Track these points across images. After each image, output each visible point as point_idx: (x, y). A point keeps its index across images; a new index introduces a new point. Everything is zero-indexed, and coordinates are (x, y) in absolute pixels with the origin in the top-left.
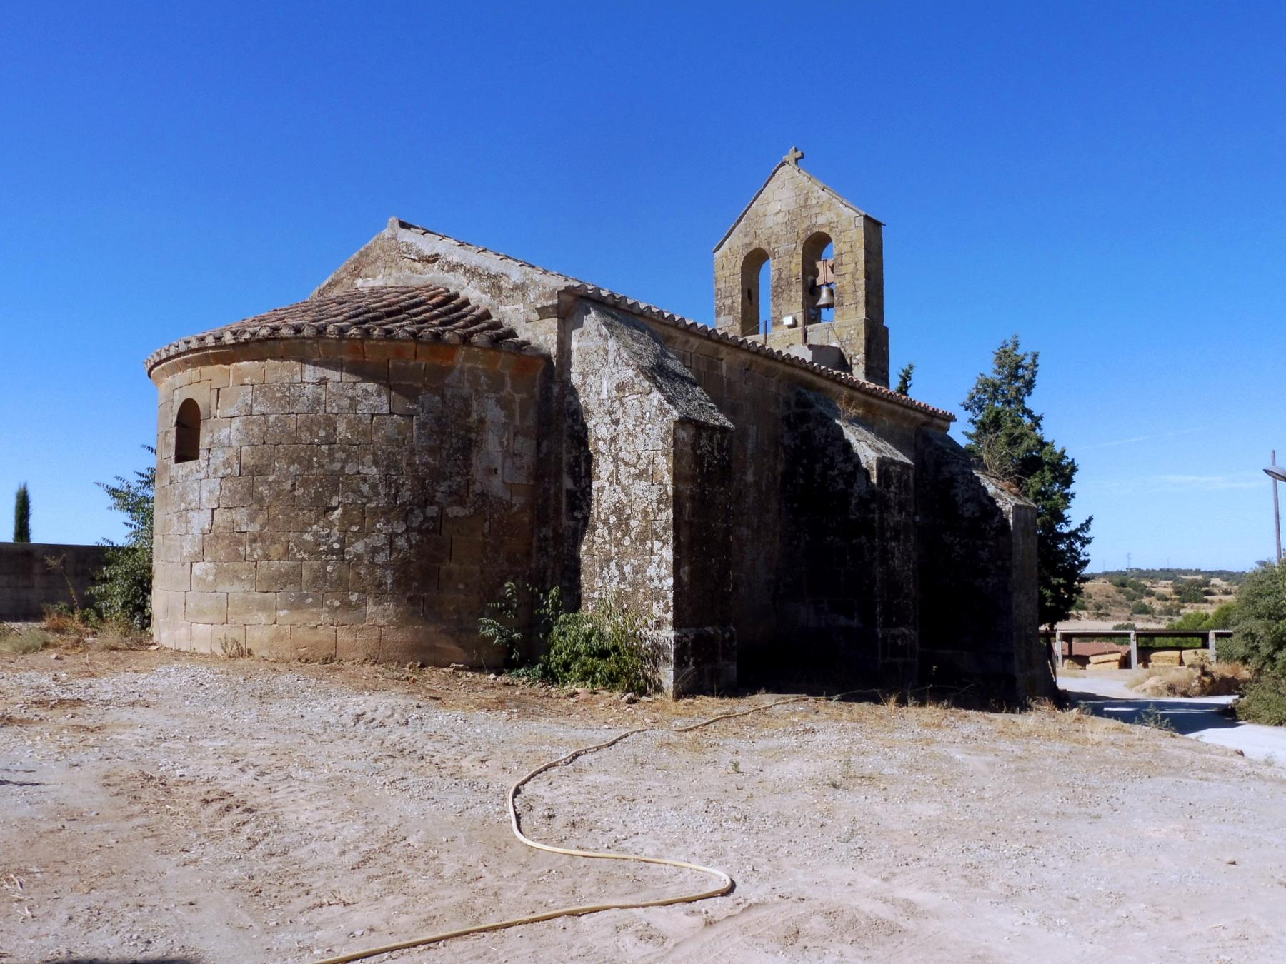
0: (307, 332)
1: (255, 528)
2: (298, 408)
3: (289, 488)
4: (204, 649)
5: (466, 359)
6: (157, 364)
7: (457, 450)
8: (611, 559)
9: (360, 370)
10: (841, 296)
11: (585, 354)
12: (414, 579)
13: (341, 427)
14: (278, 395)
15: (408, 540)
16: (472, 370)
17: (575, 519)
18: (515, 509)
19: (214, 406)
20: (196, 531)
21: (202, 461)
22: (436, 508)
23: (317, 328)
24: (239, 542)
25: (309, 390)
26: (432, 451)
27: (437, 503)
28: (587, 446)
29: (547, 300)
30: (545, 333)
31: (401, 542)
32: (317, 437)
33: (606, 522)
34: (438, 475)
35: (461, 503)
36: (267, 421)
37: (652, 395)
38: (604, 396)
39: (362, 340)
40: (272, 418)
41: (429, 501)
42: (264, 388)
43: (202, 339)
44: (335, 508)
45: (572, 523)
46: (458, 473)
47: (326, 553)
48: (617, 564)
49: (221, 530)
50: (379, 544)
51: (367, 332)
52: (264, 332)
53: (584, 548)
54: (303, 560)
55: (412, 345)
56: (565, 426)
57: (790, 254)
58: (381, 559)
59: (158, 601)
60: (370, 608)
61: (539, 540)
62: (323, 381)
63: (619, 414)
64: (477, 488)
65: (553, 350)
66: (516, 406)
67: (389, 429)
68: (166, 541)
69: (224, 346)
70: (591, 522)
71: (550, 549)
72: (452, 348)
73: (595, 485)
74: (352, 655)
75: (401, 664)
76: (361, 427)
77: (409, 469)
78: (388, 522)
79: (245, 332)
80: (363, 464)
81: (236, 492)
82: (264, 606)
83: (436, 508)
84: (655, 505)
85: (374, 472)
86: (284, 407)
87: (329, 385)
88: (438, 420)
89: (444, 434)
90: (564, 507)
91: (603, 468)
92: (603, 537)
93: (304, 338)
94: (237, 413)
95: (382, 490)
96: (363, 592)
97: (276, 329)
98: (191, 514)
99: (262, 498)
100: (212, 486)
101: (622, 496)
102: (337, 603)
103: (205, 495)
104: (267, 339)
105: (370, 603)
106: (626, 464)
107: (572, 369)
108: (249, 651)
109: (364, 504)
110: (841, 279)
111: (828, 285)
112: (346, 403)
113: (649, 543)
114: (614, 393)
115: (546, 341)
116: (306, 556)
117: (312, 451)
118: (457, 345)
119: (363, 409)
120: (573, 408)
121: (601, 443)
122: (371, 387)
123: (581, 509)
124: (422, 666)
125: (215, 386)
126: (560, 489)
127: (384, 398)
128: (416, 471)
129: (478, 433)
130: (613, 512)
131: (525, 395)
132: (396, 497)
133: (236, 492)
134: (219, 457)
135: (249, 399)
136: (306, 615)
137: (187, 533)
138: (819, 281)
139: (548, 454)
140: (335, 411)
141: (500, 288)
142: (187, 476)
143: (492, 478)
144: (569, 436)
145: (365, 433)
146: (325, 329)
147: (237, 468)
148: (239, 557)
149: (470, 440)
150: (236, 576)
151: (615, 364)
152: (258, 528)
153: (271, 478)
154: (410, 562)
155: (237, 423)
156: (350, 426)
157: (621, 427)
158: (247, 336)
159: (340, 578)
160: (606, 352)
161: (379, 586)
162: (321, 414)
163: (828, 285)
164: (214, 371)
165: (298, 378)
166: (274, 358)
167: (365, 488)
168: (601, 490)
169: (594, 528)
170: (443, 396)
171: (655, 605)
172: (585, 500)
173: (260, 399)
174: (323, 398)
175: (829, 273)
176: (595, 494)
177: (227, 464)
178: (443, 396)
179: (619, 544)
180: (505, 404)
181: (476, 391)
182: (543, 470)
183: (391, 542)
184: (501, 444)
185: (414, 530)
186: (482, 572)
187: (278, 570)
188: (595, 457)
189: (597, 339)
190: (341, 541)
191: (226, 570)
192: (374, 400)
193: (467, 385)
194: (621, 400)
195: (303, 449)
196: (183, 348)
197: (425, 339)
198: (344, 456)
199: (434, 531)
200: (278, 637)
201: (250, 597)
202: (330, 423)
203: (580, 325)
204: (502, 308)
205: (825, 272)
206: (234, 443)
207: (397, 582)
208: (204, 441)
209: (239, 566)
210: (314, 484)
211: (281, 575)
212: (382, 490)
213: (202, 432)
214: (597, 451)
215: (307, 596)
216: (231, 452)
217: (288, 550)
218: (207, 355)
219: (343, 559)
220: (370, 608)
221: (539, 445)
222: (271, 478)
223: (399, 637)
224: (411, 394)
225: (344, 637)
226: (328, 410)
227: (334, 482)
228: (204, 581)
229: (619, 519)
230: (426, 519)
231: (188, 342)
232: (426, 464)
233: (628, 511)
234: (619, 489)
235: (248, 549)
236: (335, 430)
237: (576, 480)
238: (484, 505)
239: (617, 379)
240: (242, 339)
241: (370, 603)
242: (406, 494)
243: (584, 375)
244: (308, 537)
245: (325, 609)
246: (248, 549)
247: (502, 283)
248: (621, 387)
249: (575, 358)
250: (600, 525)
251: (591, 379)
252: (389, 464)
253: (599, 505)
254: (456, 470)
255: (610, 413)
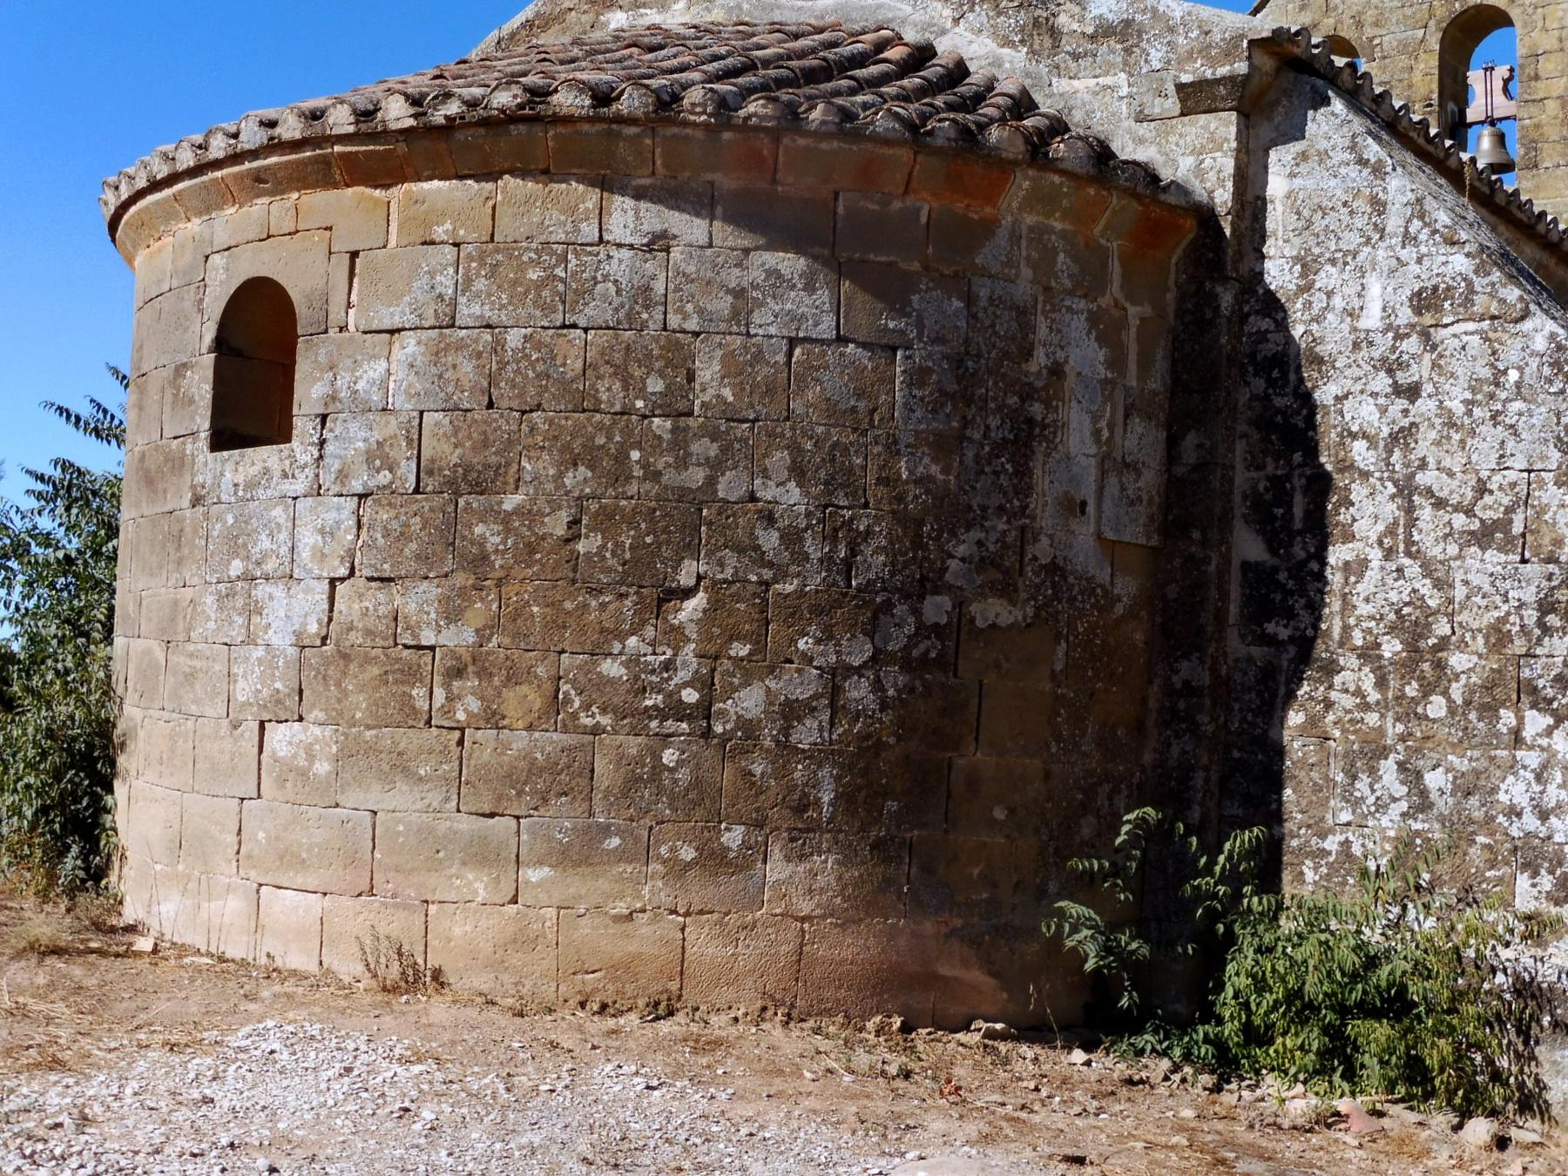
0: (630, 102)
1: (460, 637)
2: (591, 312)
3: (560, 531)
4: (299, 959)
5: (1029, 203)
6: (155, 186)
7: (999, 447)
8: (1384, 752)
9: (763, 217)
10: (1532, 145)
11: (1307, 214)
12: (886, 794)
13: (708, 371)
14: (534, 275)
15: (878, 686)
16: (1039, 232)
17: (1271, 641)
18: (1119, 609)
19: (338, 299)
20: (281, 640)
21: (301, 447)
22: (945, 602)
23: (656, 92)
24: (411, 674)
25: (620, 265)
26: (943, 446)
27: (950, 588)
28: (1312, 450)
29: (1213, 62)
30: (1198, 152)
31: (858, 691)
32: (642, 392)
33: (1369, 654)
34: (954, 513)
35: (1006, 591)
36: (498, 346)
37: (1527, 325)
38: (1372, 319)
39: (775, 135)
40: (514, 338)
41: (928, 584)
42: (491, 252)
43: (316, 115)
44: (688, 593)
45: (1257, 652)
46: (1001, 509)
47: (662, 714)
48: (1402, 766)
49: (356, 638)
50: (802, 693)
51: (792, 116)
52: (505, 99)
53: (1295, 718)
54: (596, 731)
55: (904, 154)
56: (1243, 397)
57: (1411, 50)
58: (806, 734)
59: (139, 810)
60: (777, 869)
61: (1169, 691)
62: (659, 243)
63: (1419, 371)
64: (1042, 549)
65: (1223, 197)
66: (1131, 338)
67: (832, 382)
68: (178, 660)
69: (385, 135)
70: (1320, 651)
71: (1203, 718)
72: (1002, 167)
73: (1338, 554)
74: (728, 994)
75: (854, 1022)
76: (763, 372)
77: (881, 491)
78: (827, 636)
79: (448, 95)
80: (765, 474)
81: (404, 536)
82: (481, 855)
83: (945, 602)
84: (1531, 616)
85: (790, 497)
86: (548, 309)
87: (676, 254)
88: (958, 362)
89: (968, 402)
90: (1233, 609)
91: (1366, 512)
92: (1358, 692)
93: (620, 119)
94: (410, 319)
95: (813, 548)
96: (759, 825)
97: (538, 94)
98: (262, 590)
99: (484, 557)
100: (331, 517)
101: (1425, 587)
102: (687, 853)
103: (308, 539)
104: (509, 118)
105: (776, 852)
106: (1440, 504)
107: (1269, 248)
108: (437, 974)
109: (767, 584)
110: (1533, 109)
111: (1492, 122)
112: (723, 304)
113: (1507, 717)
114: (1405, 315)
115: (1199, 171)
116: (606, 720)
117: (627, 431)
118: (1015, 163)
119: (766, 323)
120: (1269, 349)
121: (1359, 446)
122: (790, 263)
123: (1290, 614)
124: (906, 1028)
125: (342, 245)
126: (1226, 560)
127: (823, 296)
128: (900, 499)
129: (1048, 406)
130: (1392, 630)
131: (1146, 310)
132: (848, 566)
133: (404, 536)
134: (352, 438)
135: (446, 283)
136: (603, 884)
137: (250, 640)
138: (1474, 112)
139: (1202, 467)
140: (693, 324)
141: (1055, 33)
142: (251, 485)
143: (1074, 525)
144: (1255, 423)
145: (770, 391)
146: (676, 98)
147: (408, 471)
148: (409, 716)
149: (1030, 421)
150: (401, 768)
151: (1408, 239)
152: (469, 637)
153: (511, 502)
154: (879, 746)
155: (409, 346)
156: (732, 369)
157: (1425, 405)
158: (453, 108)
159: (697, 783)
160: (1379, 206)
161: (800, 809)
162: (653, 327)
163: (1492, 122)
164: (346, 204)
165: (589, 231)
166: (523, 173)
167: (770, 540)
168: (1357, 568)
169: (1331, 669)
170: (970, 299)
171: (1523, 881)
172: (1303, 592)
173: (480, 284)
174: (659, 287)
175: (1499, 98)
176: (1335, 579)
177: (378, 456)
178: (970, 299)
179: (1409, 712)
180: (1106, 329)
181: (1047, 289)
182: (1185, 507)
183: (835, 692)
184: (1097, 433)
185: (891, 658)
186: (1047, 775)
187: (527, 755)
188: (1340, 481)
189: (1353, 171)
190: (705, 684)
191: (372, 750)
192: (797, 301)
193: (1027, 273)
194: (1425, 335)
195: (600, 427)
196: (252, 136)
197: (940, 142)
198: (713, 450)
199: (942, 663)
200: (523, 940)
201: (443, 826)
202: (677, 357)
203: (1296, 132)
204: (1061, 85)
205: (1489, 93)
206: (398, 401)
207: (845, 798)
208: (309, 392)
209: (412, 739)
210: (631, 522)
211: (534, 770)
212: (813, 548)
213: (303, 367)
214: (1347, 466)
215: (606, 831)
216: (392, 425)
217: (555, 703)
218: (325, 161)
219: (707, 733)
220: (777, 869)
221: (1172, 443)
222: (511, 502)
223: (848, 948)
224: (892, 290)
225: (704, 944)
226: (674, 321)
227: (688, 520)
228: (303, 773)
229: (1412, 648)
230: (924, 630)
231: (272, 124)
232: (923, 481)
233: (1442, 628)
234: (1413, 568)
235: (440, 695)
236: (691, 377)
237: (1275, 534)
238: (1056, 596)
239: (1415, 277)
240: (438, 117)
241: (776, 852)
242: (873, 561)
243: (1307, 266)
244: (612, 668)
245: (655, 867)
246: (440, 695)
247: (1062, 19)
248: (1426, 301)
249: (1276, 218)
250: (1350, 661)
251: (1328, 277)
252: (832, 477)
253: (1347, 606)
254: (996, 500)
255: (1390, 366)
